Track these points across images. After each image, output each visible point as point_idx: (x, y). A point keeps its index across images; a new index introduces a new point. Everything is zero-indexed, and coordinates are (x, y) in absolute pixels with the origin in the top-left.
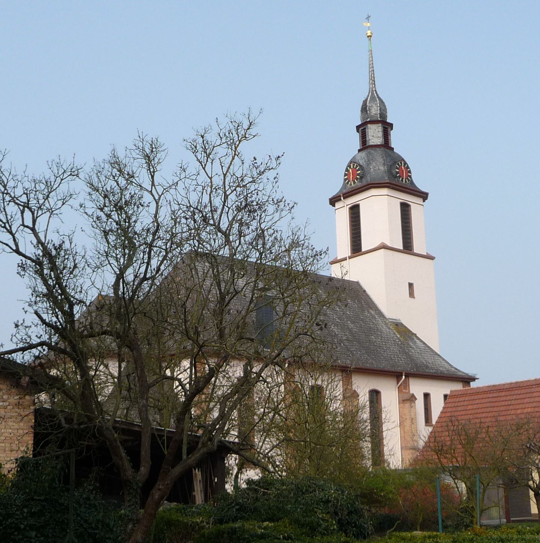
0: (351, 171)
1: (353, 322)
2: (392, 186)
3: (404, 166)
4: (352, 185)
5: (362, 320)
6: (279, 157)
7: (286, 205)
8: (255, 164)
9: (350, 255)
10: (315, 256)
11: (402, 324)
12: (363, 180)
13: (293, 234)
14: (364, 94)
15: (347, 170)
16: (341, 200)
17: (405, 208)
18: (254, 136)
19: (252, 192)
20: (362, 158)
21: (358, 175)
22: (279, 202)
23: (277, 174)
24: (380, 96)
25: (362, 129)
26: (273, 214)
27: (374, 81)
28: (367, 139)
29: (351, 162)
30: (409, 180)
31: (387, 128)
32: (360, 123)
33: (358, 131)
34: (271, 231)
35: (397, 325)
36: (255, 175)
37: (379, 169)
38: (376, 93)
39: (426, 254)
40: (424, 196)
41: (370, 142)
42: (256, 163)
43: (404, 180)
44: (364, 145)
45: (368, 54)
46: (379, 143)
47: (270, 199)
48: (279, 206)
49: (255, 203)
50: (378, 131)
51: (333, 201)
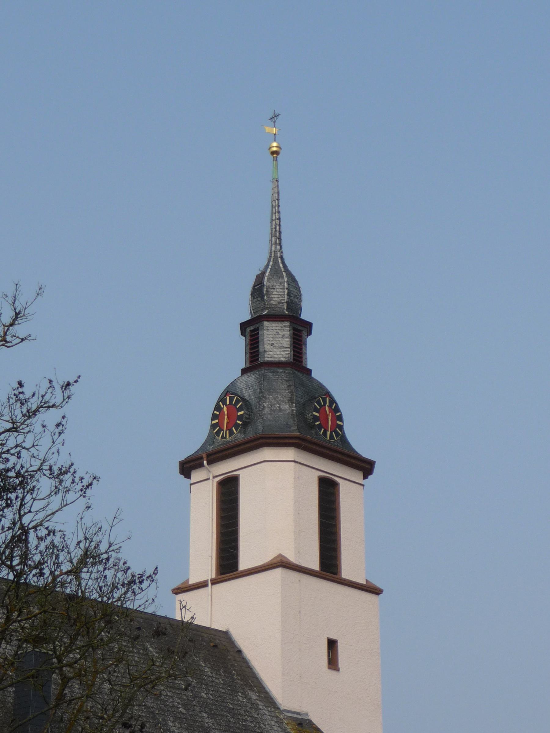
0: (225, 409)
1: (212, 715)
2: (304, 444)
3: (330, 406)
4: (226, 438)
5: (231, 711)
6: (68, 384)
7: (77, 480)
8: (21, 396)
9: (214, 576)
10: (130, 583)
11: (310, 723)
12: (249, 429)
13: (86, 539)
14: (259, 261)
15: (218, 408)
16: (201, 465)
17: (328, 490)
18: (22, 340)
19: (8, 451)
20: (248, 386)
21: (240, 418)
22: (63, 472)
23: (63, 417)
24: (289, 268)
25: (251, 330)
26: (50, 496)
27: (280, 239)
28: (261, 350)
29: (226, 392)
30: (337, 434)
31: (300, 331)
32: (247, 317)
33: (243, 333)
34: (42, 532)
35: (300, 724)
36: (19, 418)
37: (280, 410)
38: (283, 263)
39: (364, 582)
40: (366, 467)
41: (266, 355)
42: (22, 393)
43: (328, 433)
44: (255, 361)
45: (271, 185)
46: (283, 359)
47: (46, 467)
48: (61, 482)
49: (12, 474)
50: (283, 336)
51: (187, 467)
